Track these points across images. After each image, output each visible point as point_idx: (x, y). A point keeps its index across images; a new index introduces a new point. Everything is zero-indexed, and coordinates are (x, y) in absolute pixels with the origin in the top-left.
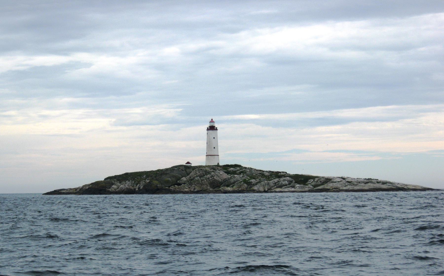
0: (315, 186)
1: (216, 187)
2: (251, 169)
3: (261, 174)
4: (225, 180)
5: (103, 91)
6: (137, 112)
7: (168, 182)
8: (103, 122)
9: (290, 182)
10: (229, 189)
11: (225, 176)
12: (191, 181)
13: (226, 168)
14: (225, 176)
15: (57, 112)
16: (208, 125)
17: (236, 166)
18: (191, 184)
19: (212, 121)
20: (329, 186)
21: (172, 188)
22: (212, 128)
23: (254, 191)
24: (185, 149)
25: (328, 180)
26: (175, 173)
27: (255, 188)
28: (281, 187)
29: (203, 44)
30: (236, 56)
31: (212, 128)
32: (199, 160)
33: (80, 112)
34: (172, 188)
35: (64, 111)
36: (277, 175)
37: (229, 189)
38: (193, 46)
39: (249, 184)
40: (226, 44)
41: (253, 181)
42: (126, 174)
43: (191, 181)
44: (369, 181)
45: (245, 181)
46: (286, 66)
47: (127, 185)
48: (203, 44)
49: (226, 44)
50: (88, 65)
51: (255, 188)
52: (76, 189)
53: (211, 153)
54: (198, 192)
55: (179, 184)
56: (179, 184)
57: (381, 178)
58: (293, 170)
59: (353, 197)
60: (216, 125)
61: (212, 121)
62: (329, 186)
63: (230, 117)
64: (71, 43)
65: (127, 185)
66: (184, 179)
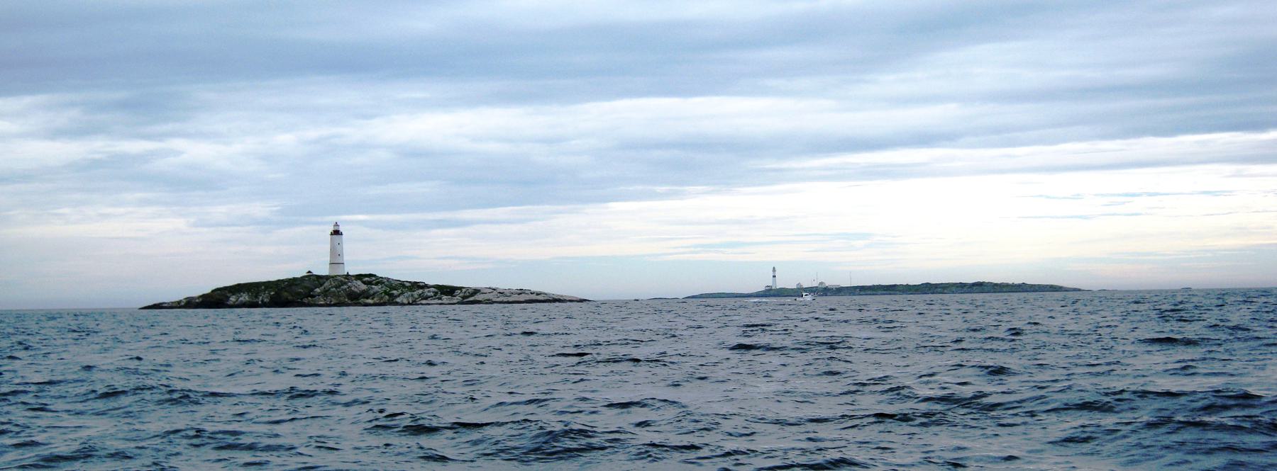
0: (464, 298)
1: (355, 299)
2: (388, 279)
3: (402, 285)
4: (364, 292)
5: (189, 185)
6: (220, 211)
7: (299, 294)
8: (180, 223)
9: (436, 293)
10: (370, 301)
11: (364, 287)
12: (326, 293)
13: (359, 277)
14: (364, 287)
15: (122, 210)
16: (332, 229)
17: (370, 275)
18: (326, 296)
19: (336, 224)
20: (478, 297)
21: (305, 301)
22: (336, 233)
23: (397, 304)
24: (296, 255)
25: (476, 291)
26: (307, 284)
27: (398, 300)
28: (426, 298)
29: (325, 131)
30: (361, 147)
31: (336, 233)
32: (322, 269)
33: (149, 210)
34: (305, 301)
35: (130, 209)
36: (415, 286)
37: (370, 301)
38: (312, 133)
39: (391, 295)
40: (352, 132)
41: (395, 292)
42: (239, 285)
43: (326, 293)
44: (521, 292)
45: (385, 292)
46: (421, 162)
47: (245, 297)
48: (325, 131)
49: (352, 132)
50: (178, 153)
51: (398, 300)
52: (179, 302)
53: (336, 258)
54: (335, 305)
55: (313, 296)
56: (313, 296)
57: (533, 289)
58: (433, 279)
59: (354, 321)
60: (341, 229)
61: (336, 224)
62: (478, 297)
63: (319, 219)
64: (170, 127)
65: (245, 297)
66: (318, 290)
